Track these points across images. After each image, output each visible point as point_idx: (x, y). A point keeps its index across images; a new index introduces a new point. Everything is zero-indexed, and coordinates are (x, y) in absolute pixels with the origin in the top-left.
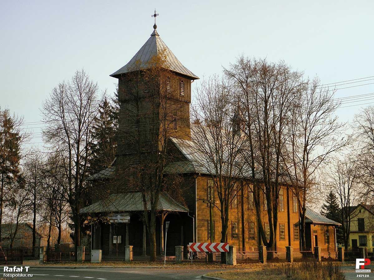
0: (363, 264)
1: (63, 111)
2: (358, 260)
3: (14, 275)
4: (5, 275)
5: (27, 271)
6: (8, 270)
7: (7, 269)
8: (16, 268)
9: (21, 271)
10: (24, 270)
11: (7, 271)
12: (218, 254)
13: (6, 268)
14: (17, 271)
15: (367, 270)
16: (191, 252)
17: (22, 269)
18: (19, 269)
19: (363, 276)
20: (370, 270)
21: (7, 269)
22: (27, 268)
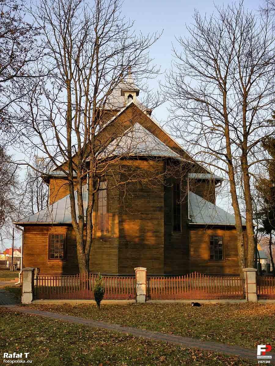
0: (264, 350)
2: (259, 347)
3: (13, 362)
5: (26, 357)
6: (8, 356)
7: (7, 356)
9: (21, 357)
10: (24, 356)
11: (7, 357)
13: (6, 354)
14: (16, 357)
15: (268, 356)
16: (246, 266)
18: (18, 355)
19: (264, 362)
21: (7, 356)
22: (26, 354)
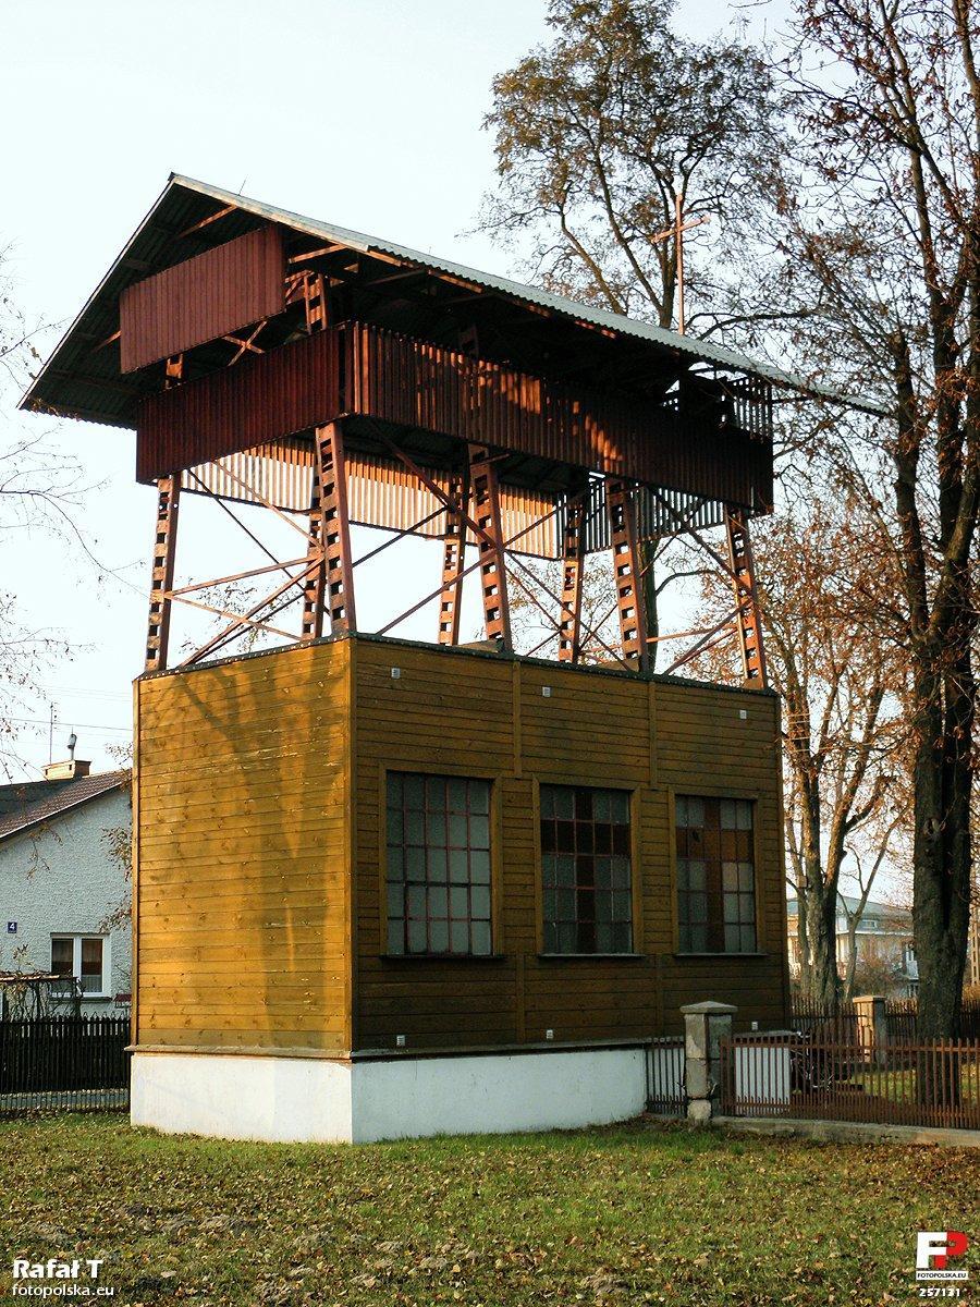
0: (942, 1251)
1: (532, 597)
2: (924, 1239)
3: (48, 1291)
4: (17, 1291)
8: (55, 1266)
9: (75, 1275)
11: (25, 1275)
12: (891, 1084)
13: (21, 1265)
14: (59, 1274)
17: (78, 1267)
19: (941, 1292)
20: (967, 1272)
21: (23, 1270)
